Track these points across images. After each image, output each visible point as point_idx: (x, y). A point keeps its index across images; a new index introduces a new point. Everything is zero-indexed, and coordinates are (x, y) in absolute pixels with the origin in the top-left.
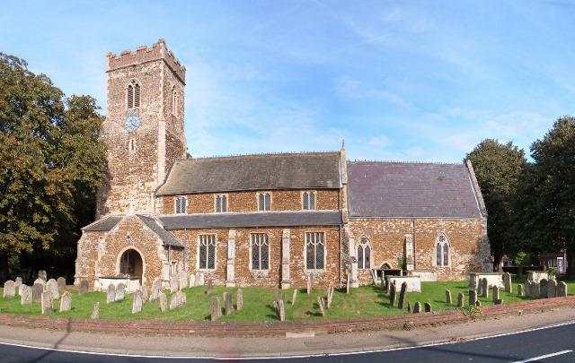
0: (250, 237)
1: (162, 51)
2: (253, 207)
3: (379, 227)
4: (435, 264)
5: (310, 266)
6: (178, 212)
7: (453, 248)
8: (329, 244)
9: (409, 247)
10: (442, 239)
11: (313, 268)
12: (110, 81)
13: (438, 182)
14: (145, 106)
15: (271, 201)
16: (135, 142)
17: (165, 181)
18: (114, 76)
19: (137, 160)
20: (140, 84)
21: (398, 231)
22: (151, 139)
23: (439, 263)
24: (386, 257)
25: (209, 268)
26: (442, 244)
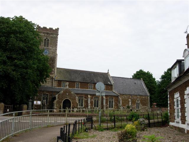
0: (94, 97)
3: (122, 97)
8: (115, 101)
9: (130, 103)
10: (138, 101)
11: (110, 107)
14: (51, 48)
15: (93, 87)
20: (50, 40)
25: (112, 108)
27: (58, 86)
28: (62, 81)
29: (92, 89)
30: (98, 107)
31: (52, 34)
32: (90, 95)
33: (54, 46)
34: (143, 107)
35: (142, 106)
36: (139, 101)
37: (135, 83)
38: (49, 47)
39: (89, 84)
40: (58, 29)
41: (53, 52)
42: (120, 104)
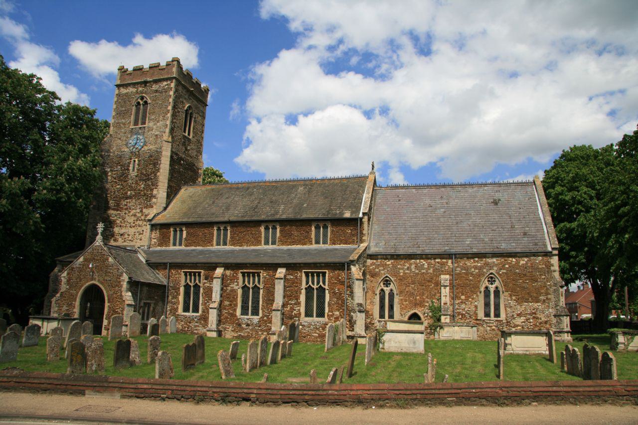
0: (240, 275)
1: (174, 70)
2: (258, 243)
3: (407, 265)
4: (481, 314)
5: (308, 314)
6: (174, 244)
7: (507, 294)
9: (445, 292)
10: (492, 280)
12: (118, 95)
13: (492, 207)
14: (151, 124)
15: (278, 234)
16: (137, 162)
17: (165, 209)
18: (124, 91)
19: (137, 183)
21: (431, 271)
22: (153, 160)
23: (487, 315)
24: (416, 305)
26: (492, 288)
27: (160, 245)
30: (257, 314)
34: (519, 309)
35: (512, 303)
41: (156, 135)
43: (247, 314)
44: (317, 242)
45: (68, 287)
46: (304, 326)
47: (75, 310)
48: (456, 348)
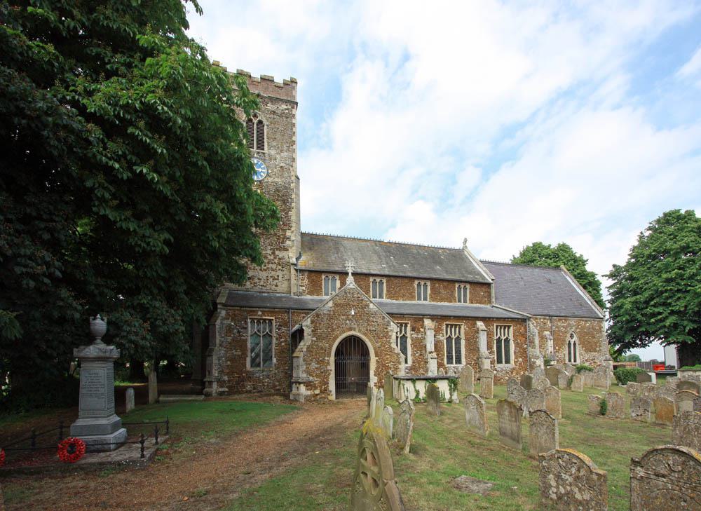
0: (444, 327)
10: (572, 337)
14: (273, 152)
15: (429, 291)
20: (265, 122)
27: (311, 293)
28: (321, 272)
29: (425, 299)
31: (274, 100)
32: (433, 317)
33: (285, 148)
36: (575, 338)
37: (550, 281)
38: (266, 150)
39: (416, 282)
40: (294, 82)
42: (534, 347)
43: (452, 363)
44: (460, 301)
45: (314, 339)
46: (498, 371)
47: (329, 368)
48: (317, 395)
